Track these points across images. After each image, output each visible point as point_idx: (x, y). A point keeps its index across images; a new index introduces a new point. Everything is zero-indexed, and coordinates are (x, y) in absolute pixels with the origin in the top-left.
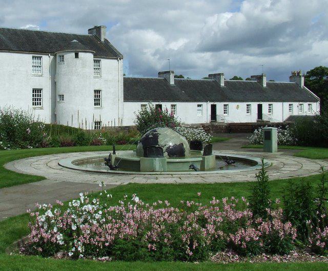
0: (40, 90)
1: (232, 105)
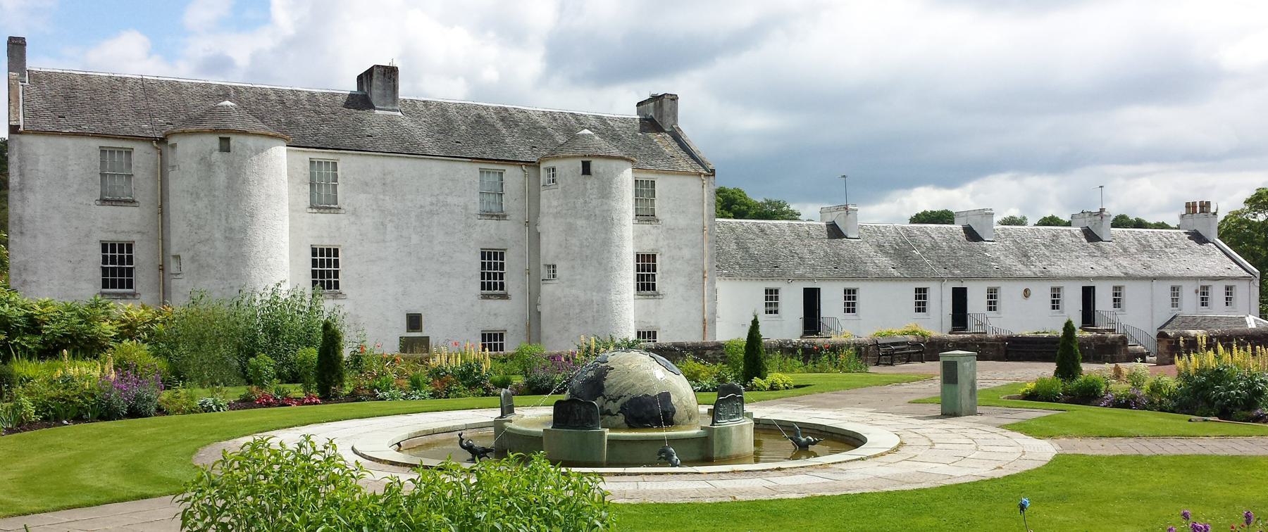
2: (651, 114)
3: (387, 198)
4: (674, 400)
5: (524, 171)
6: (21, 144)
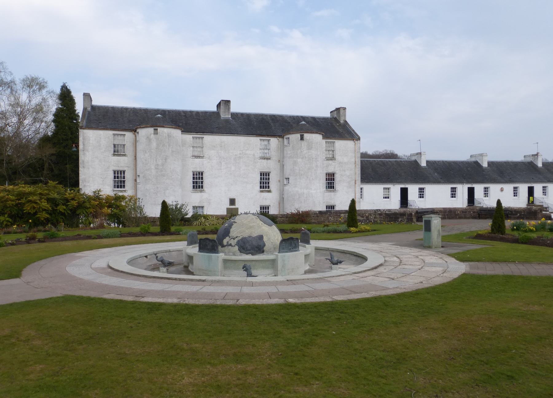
0: (268, 174)
1: (429, 188)
2: (336, 116)
3: (222, 152)
4: (265, 239)
5: (278, 140)
6: (83, 133)
